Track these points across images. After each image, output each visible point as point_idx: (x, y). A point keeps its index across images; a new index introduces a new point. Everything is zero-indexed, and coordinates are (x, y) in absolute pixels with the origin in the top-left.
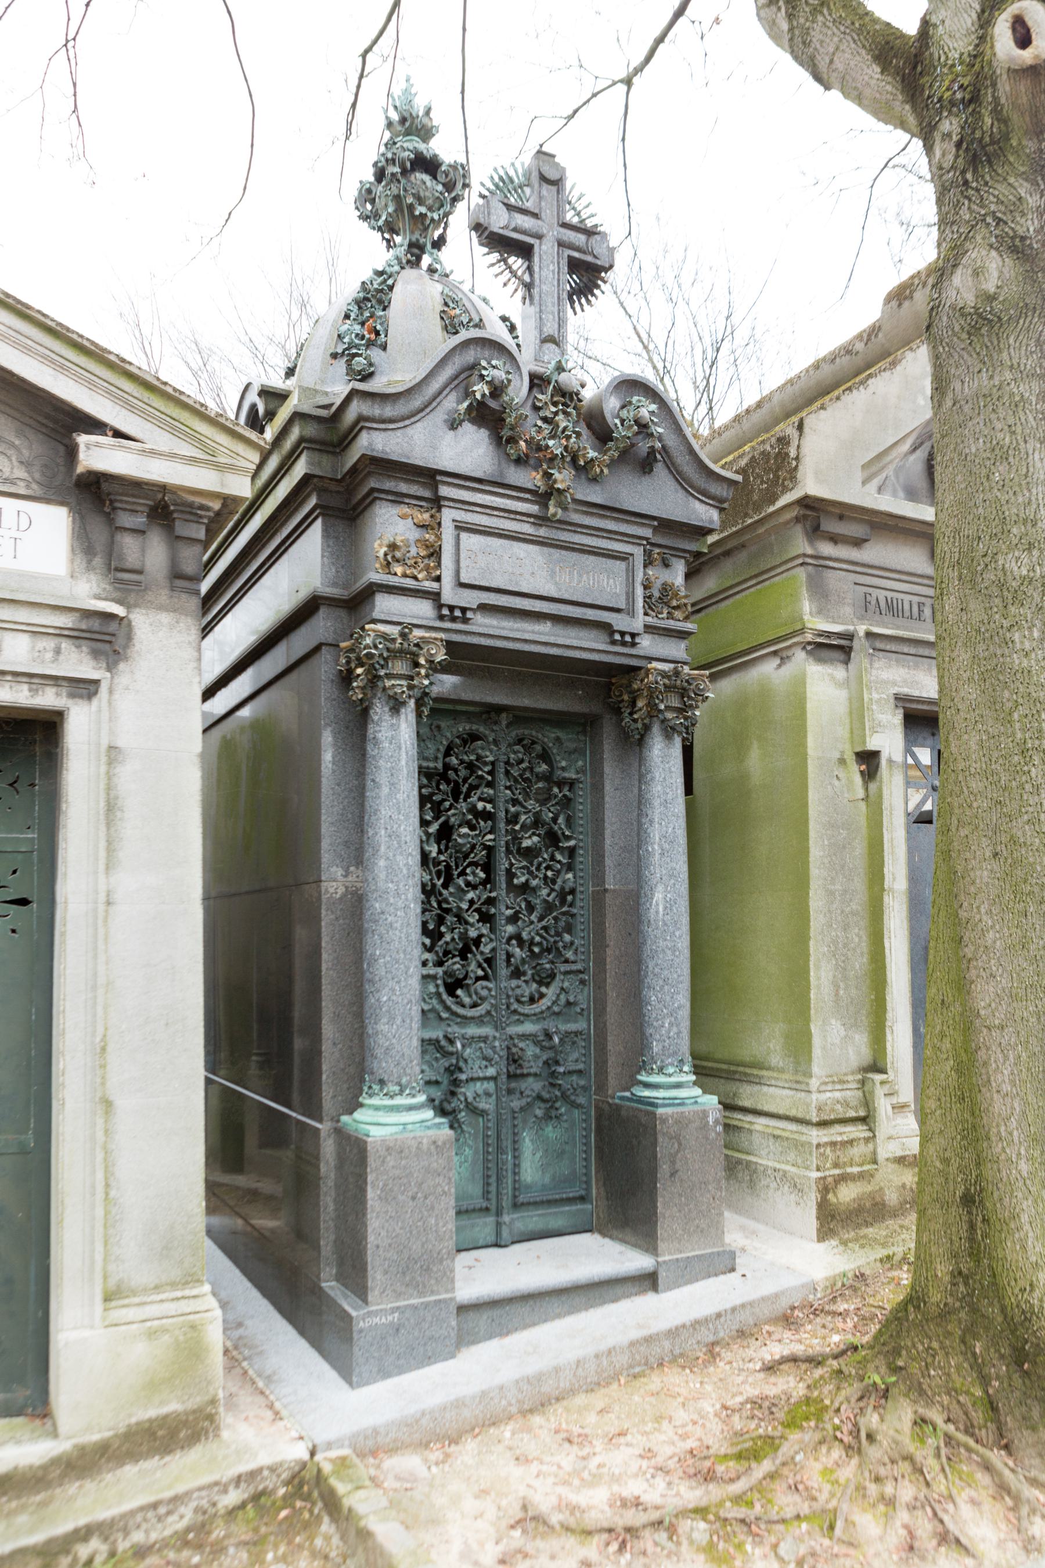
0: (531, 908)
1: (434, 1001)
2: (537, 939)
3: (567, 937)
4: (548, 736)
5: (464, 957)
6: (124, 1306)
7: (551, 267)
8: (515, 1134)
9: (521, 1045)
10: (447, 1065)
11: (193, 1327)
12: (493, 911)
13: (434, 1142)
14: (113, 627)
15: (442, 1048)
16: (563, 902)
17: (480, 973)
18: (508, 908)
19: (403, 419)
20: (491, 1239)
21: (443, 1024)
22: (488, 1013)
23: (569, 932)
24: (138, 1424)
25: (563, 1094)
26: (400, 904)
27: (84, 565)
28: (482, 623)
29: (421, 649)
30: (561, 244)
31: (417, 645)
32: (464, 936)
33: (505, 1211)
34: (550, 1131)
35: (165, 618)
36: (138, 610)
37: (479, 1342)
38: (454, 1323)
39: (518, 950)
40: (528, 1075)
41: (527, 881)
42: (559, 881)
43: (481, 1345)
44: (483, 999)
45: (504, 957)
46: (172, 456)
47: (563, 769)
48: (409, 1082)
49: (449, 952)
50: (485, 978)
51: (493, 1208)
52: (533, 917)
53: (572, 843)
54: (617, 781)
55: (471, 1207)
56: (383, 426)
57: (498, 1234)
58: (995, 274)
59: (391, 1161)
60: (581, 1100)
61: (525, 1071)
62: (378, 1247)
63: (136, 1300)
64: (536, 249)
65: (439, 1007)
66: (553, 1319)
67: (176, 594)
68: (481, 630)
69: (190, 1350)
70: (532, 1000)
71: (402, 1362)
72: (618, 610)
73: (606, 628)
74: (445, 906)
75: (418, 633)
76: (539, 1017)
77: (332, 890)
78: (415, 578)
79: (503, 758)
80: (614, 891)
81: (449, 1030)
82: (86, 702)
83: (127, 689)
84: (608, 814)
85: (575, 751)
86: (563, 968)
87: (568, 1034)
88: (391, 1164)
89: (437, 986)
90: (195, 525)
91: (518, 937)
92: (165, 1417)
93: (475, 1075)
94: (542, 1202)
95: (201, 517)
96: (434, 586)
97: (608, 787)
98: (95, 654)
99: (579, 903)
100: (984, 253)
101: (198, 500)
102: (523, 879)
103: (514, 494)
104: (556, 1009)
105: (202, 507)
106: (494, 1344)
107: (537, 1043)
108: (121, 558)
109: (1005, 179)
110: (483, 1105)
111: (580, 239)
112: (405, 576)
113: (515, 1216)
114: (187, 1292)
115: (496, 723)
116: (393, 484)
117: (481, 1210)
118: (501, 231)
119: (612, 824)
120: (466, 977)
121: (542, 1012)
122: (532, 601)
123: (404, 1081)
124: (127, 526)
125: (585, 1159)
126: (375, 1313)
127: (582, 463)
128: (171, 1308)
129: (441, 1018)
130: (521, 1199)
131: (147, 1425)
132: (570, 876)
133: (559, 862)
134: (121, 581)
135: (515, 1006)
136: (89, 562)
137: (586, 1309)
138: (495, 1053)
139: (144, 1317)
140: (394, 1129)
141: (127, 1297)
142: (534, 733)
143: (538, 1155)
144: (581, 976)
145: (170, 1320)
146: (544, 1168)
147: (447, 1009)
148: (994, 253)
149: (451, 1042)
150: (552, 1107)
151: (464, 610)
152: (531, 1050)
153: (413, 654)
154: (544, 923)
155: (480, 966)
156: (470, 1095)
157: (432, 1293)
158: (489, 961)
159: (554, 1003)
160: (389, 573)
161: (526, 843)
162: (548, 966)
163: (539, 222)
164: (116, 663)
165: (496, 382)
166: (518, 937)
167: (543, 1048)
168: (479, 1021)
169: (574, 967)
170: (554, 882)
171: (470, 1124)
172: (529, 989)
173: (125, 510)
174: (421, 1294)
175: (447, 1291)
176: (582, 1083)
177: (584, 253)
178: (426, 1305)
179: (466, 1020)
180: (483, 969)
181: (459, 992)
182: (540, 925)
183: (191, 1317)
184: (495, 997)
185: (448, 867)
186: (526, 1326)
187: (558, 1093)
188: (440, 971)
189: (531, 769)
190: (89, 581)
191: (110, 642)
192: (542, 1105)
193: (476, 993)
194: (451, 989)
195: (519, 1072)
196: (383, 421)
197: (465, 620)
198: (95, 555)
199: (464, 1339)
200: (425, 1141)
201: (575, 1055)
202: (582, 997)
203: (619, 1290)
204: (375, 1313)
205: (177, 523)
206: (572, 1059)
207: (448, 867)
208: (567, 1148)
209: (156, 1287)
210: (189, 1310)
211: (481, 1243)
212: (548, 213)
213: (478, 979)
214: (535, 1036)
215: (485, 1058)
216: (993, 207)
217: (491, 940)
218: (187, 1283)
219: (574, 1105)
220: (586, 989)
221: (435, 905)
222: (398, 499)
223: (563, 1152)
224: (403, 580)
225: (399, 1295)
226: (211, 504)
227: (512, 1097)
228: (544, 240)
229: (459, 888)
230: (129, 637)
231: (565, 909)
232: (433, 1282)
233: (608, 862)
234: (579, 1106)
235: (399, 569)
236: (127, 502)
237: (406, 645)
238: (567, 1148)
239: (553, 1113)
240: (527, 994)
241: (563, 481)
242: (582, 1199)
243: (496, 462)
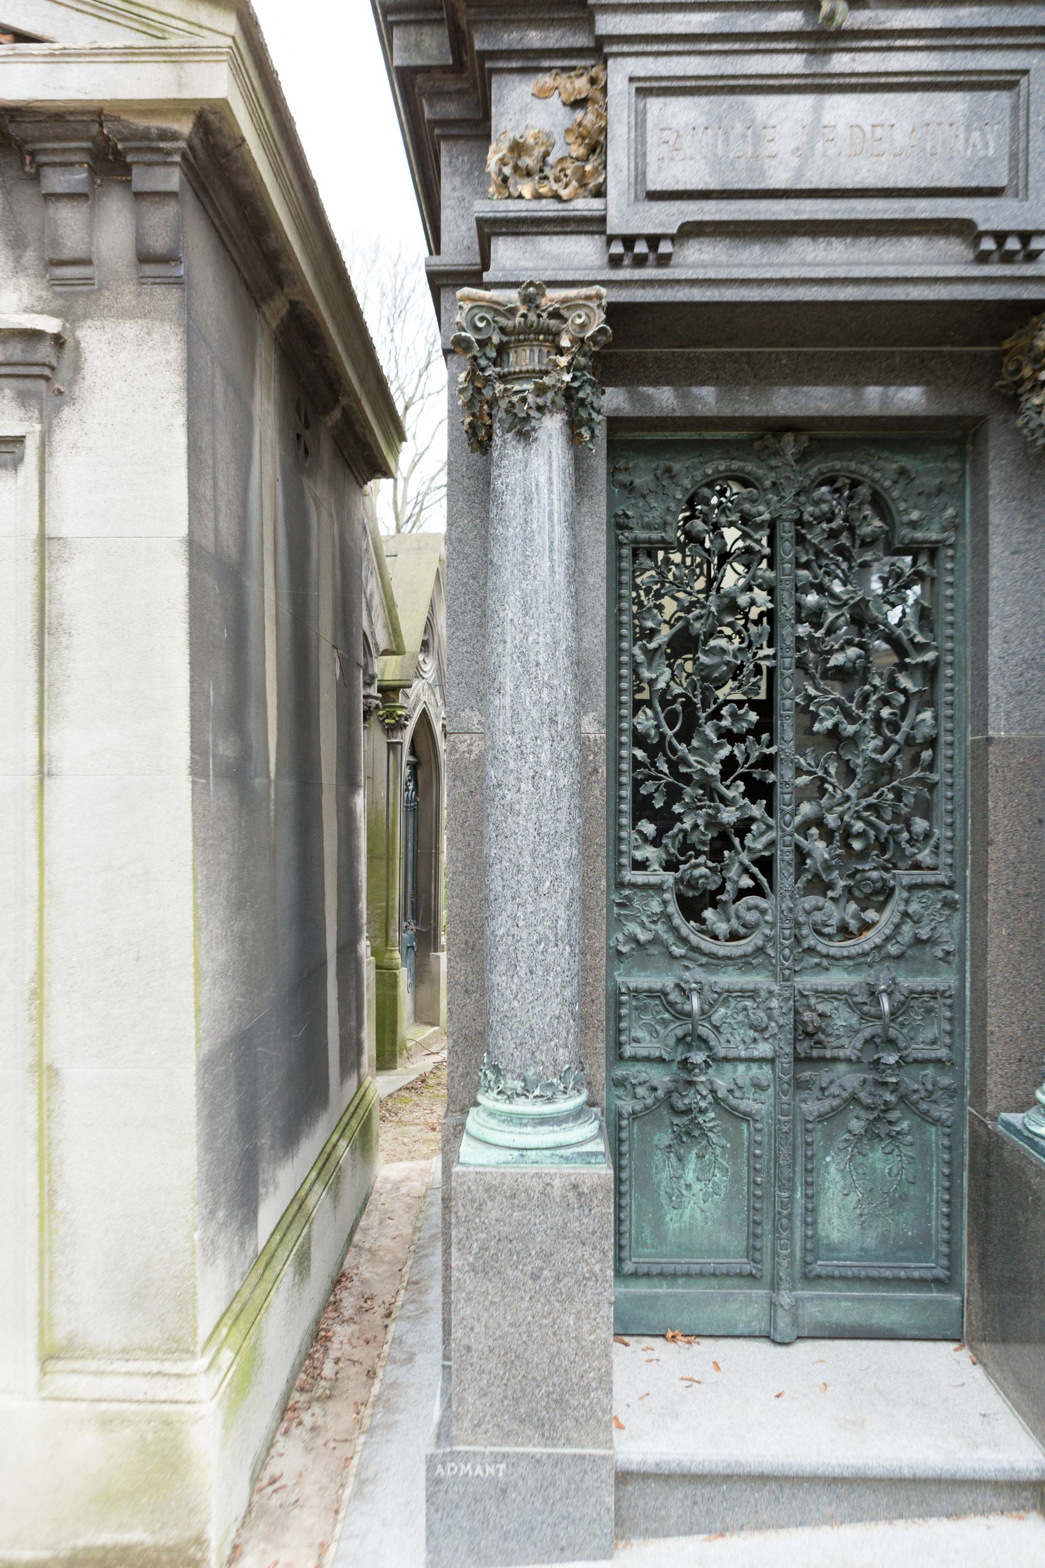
0: (849, 773)
1: (660, 928)
2: (858, 826)
3: (920, 825)
4: (882, 470)
5: (715, 855)
6: (74, 1371)
8: (809, 1158)
9: (821, 1008)
10: (680, 1032)
11: (168, 1423)
12: (771, 777)
13: (575, 1187)
14: (44, 352)
15: (672, 1004)
16: (915, 761)
17: (746, 882)
18: (799, 771)
20: (760, 1326)
21: (677, 966)
22: (760, 950)
23: (927, 816)
24: (87, 1549)
25: (902, 1098)
26: (527, 772)
27: (11, 264)
28: (699, 259)
29: (565, 320)
31: (555, 314)
32: (712, 822)
33: (784, 1285)
34: (877, 1157)
35: (130, 329)
36: (89, 322)
37: (667, 1535)
38: (610, 1500)
39: (821, 845)
40: (835, 1060)
41: (836, 726)
42: (905, 726)
43: (670, 1542)
44: (751, 928)
45: (790, 857)
46: (97, 53)
47: (914, 525)
48: (539, 1077)
49: (692, 847)
50: (757, 890)
51: (767, 1278)
52: (851, 791)
53: (929, 656)
54: (1016, 538)
55: (724, 1269)
57: (772, 1320)
59: (493, 1211)
60: (943, 1112)
61: (828, 1054)
62: (469, 1349)
63: (92, 1365)
65: (668, 937)
66: (817, 1523)
67: (147, 288)
68: (691, 274)
69: (164, 1459)
70: (844, 931)
71: (511, 1545)
72: (994, 192)
73: (962, 229)
74: (683, 770)
75: (554, 294)
76: (858, 961)
77: (463, 747)
78: (557, 197)
79: (790, 513)
80: (1008, 741)
81: (687, 975)
82: (10, 474)
83: (75, 446)
84: (995, 599)
85: (940, 490)
86: (907, 877)
87: (914, 994)
88: (494, 1215)
89: (665, 903)
90: (162, 170)
91: (819, 822)
92: (127, 1549)
93: (732, 1054)
94: (857, 1279)
95: (168, 153)
96: (595, 205)
97: (997, 549)
98: (23, 398)
99: (943, 764)
101: (155, 124)
102: (829, 724)
104: (893, 949)
105: (166, 135)
106: (692, 1546)
107: (854, 1007)
108: (55, 243)
110: (748, 1104)
112: (538, 196)
113: (807, 1293)
114: (168, 1367)
115: (776, 454)
116: (515, 35)
117: (740, 1275)
119: (1004, 618)
120: (721, 889)
121: (865, 954)
122: (794, 203)
123: (531, 1073)
124: (59, 190)
125: (948, 1216)
126: (466, 1457)
128: (140, 1387)
129: (673, 957)
130: (820, 1266)
131: (100, 1555)
132: (927, 715)
133: (904, 691)
134: (63, 282)
135: (812, 940)
136: (18, 259)
137: (889, 1519)
138: (770, 1018)
139: (97, 1396)
140: (503, 1155)
141: (82, 1357)
142: (853, 465)
143: (854, 1198)
144: (946, 893)
145: (134, 1407)
146: (864, 1221)
147: (684, 941)
149: (686, 994)
150: (878, 1119)
151: (653, 241)
152: (843, 1018)
153: (547, 331)
154: (872, 800)
155: (746, 870)
156: (722, 1085)
157: (569, 1441)
158: (766, 865)
159: (888, 939)
160: (510, 197)
161: (837, 660)
162: (875, 875)
164: (57, 409)
166: (819, 822)
167: (864, 1016)
168: (744, 963)
169: (930, 878)
170: (895, 728)
171: (724, 1133)
172: (834, 914)
173: (53, 165)
174: (549, 1440)
175: (596, 1444)
176: (946, 1081)
178: (558, 1461)
179: (716, 962)
180: (753, 877)
181: (708, 914)
182: (864, 803)
183: (166, 1408)
184: (772, 925)
185: (689, 704)
186: (760, 1527)
187: (889, 1097)
188: (669, 877)
189: (852, 530)
190: (17, 289)
191: (47, 379)
192: (863, 1114)
193: (738, 917)
194: (691, 909)
195: (815, 1053)
197: (664, 261)
198: (26, 247)
199: (625, 1526)
200: (557, 1183)
201: (931, 1033)
202: (949, 932)
203: (964, 1498)
204: (466, 1457)
205: (135, 170)
206: (925, 1039)
207: (689, 704)
208: (912, 1191)
209: (125, 1350)
210: (163, 1396)
211: (741, 1329)
213: (742, 893)
214: (849, 994)
215: (753, 1027)
217: (769, 828)
218: (169, 1351)
219: (926, 1117)
220: (957, 917)
221: (665, 768)
222: (530, 63)
223: (904, 1197)
224: (535, 205)
225: (507, 1436)
226: (175, 126)
227: (805, 1094)
229: (708, 742)
230: (77, 367)
231: (917, 774)
232: (570, 1423)
233: (994, 687)
234: (936, 1122)
235: (526, 188)
236: (54, 151)
237: (532, 317)
238: (912, 1191)
239: (883, 1129)
240: (833, 921)
242: (940, 1283)
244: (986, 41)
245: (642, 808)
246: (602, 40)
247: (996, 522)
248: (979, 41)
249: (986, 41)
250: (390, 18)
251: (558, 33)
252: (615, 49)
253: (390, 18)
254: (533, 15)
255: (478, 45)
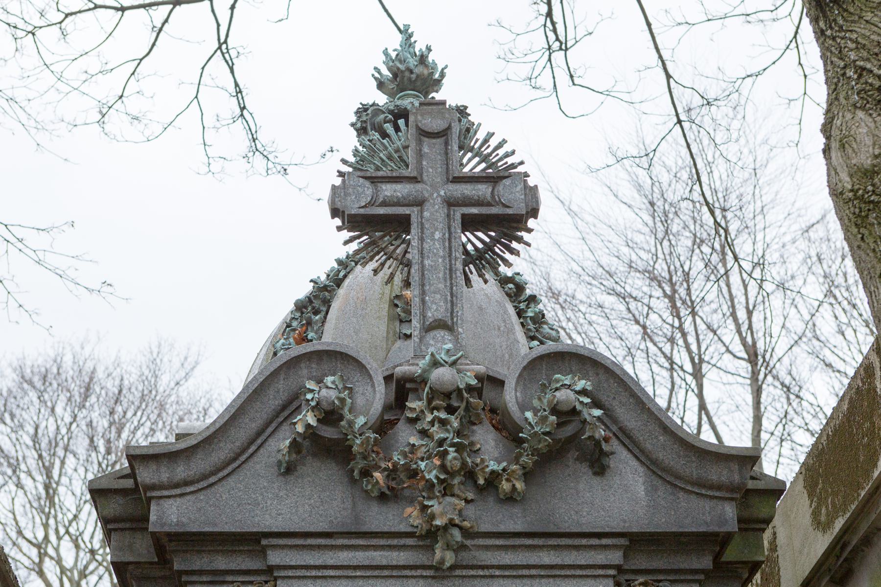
7: (437, 235)
19: (205, 477)
30: (451, 203)
56: (178, 491)
58: (869, 141)
64: (414, 219)
100: (849, 116)
103: (382, 542)
109: (860, 17)
111: (483, 190)
118: (362, 211)
127: (481, 481)
148: (860, 114)
163: (419, 186)
165: (324, 405)
177: (489, 204)
196: (177, 486)
212: (433, 171)
216: (853, 56)
228: (427, 206)
241: (442, 514)
243: (348, 504)
244: (563, 573)
245: (533, 338)
246: (270, 569)
247: (771, 428)
248: (558, 572)
249: (563, 573)
250: (109, 527)
251: (240, 559)
252: (283, 573)
253: (109, 527)
254: (220, 548)
255: (176, 567)
